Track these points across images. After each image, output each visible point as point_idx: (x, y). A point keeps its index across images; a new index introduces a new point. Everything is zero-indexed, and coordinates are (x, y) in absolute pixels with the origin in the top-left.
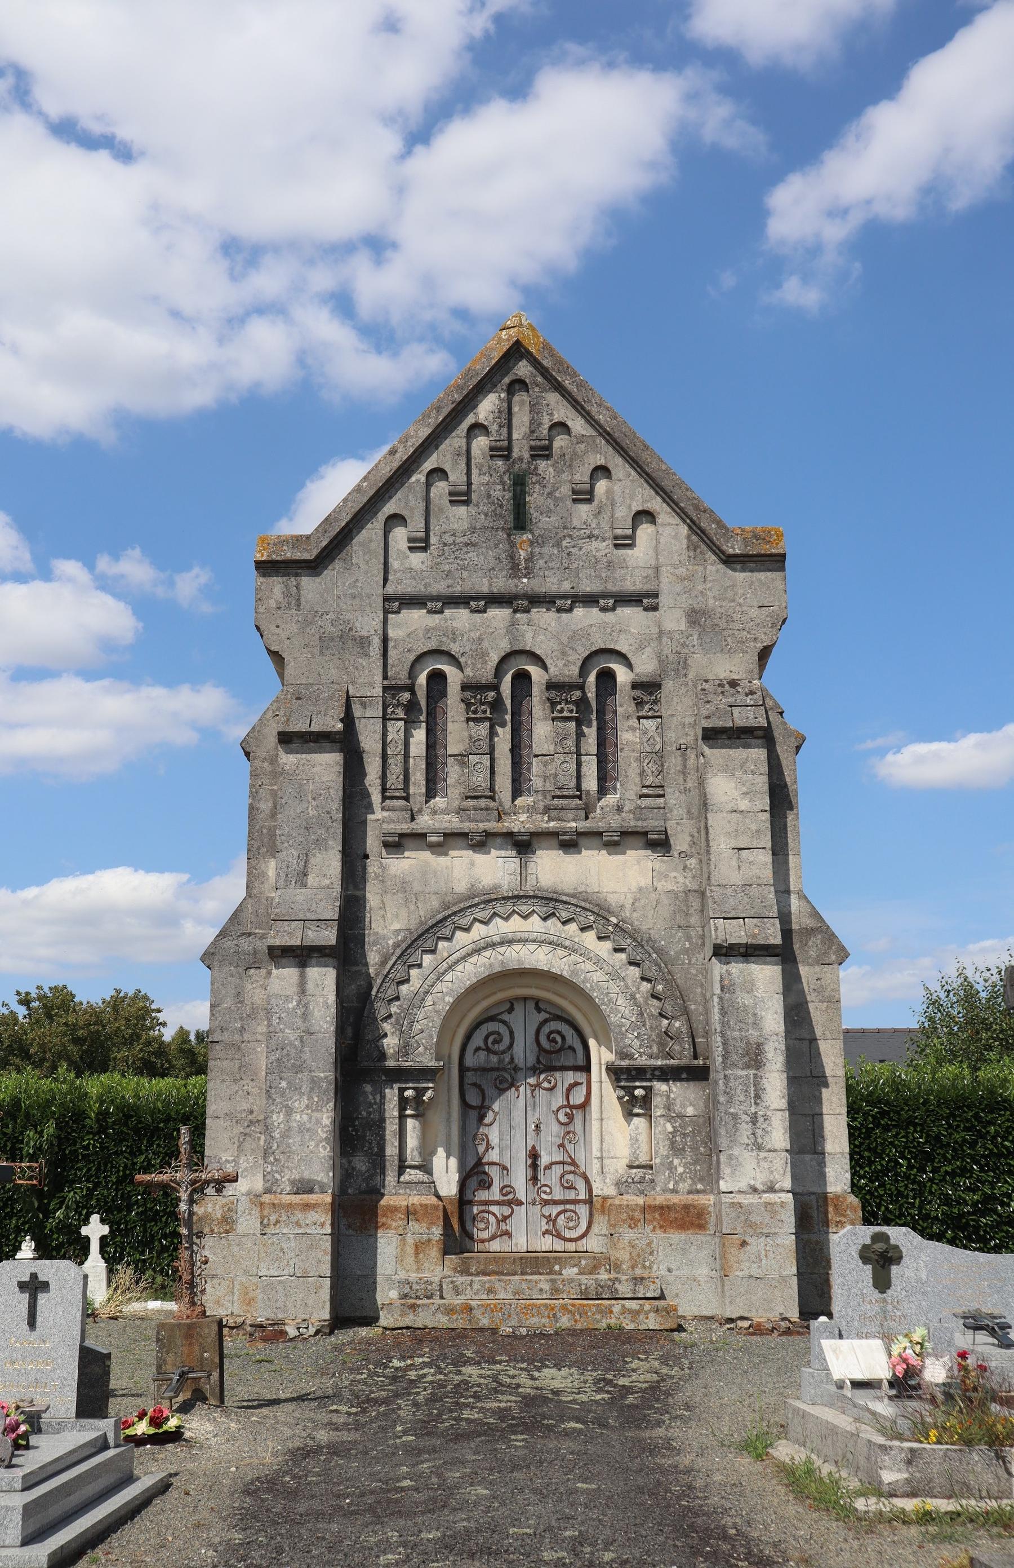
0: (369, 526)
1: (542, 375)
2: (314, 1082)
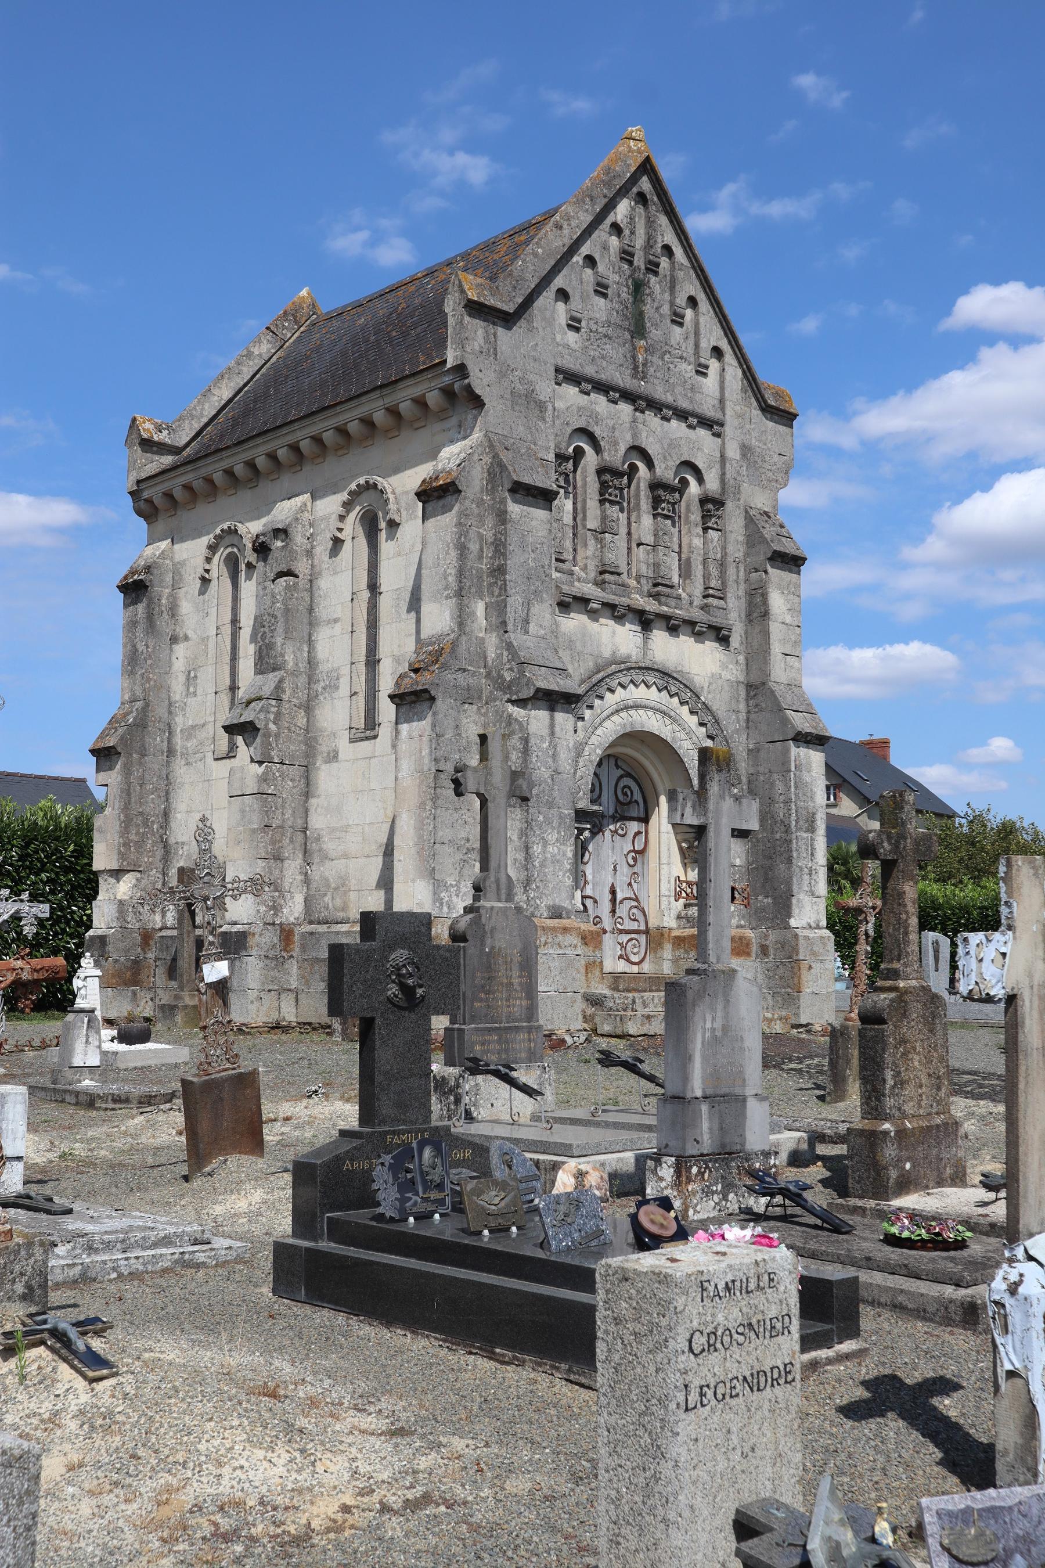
0: (545, 293)
1: (658, 196)
2: (561, 817)
